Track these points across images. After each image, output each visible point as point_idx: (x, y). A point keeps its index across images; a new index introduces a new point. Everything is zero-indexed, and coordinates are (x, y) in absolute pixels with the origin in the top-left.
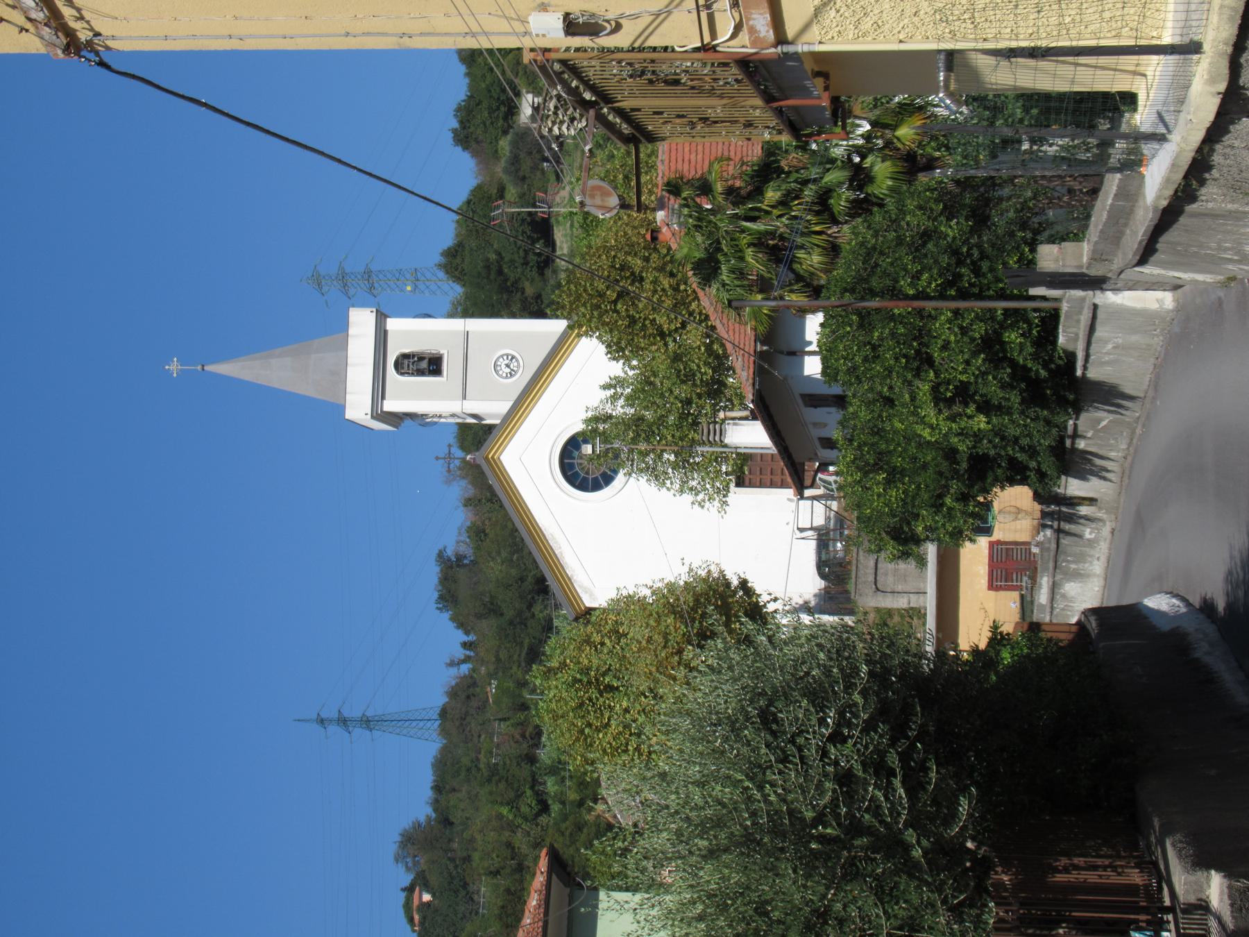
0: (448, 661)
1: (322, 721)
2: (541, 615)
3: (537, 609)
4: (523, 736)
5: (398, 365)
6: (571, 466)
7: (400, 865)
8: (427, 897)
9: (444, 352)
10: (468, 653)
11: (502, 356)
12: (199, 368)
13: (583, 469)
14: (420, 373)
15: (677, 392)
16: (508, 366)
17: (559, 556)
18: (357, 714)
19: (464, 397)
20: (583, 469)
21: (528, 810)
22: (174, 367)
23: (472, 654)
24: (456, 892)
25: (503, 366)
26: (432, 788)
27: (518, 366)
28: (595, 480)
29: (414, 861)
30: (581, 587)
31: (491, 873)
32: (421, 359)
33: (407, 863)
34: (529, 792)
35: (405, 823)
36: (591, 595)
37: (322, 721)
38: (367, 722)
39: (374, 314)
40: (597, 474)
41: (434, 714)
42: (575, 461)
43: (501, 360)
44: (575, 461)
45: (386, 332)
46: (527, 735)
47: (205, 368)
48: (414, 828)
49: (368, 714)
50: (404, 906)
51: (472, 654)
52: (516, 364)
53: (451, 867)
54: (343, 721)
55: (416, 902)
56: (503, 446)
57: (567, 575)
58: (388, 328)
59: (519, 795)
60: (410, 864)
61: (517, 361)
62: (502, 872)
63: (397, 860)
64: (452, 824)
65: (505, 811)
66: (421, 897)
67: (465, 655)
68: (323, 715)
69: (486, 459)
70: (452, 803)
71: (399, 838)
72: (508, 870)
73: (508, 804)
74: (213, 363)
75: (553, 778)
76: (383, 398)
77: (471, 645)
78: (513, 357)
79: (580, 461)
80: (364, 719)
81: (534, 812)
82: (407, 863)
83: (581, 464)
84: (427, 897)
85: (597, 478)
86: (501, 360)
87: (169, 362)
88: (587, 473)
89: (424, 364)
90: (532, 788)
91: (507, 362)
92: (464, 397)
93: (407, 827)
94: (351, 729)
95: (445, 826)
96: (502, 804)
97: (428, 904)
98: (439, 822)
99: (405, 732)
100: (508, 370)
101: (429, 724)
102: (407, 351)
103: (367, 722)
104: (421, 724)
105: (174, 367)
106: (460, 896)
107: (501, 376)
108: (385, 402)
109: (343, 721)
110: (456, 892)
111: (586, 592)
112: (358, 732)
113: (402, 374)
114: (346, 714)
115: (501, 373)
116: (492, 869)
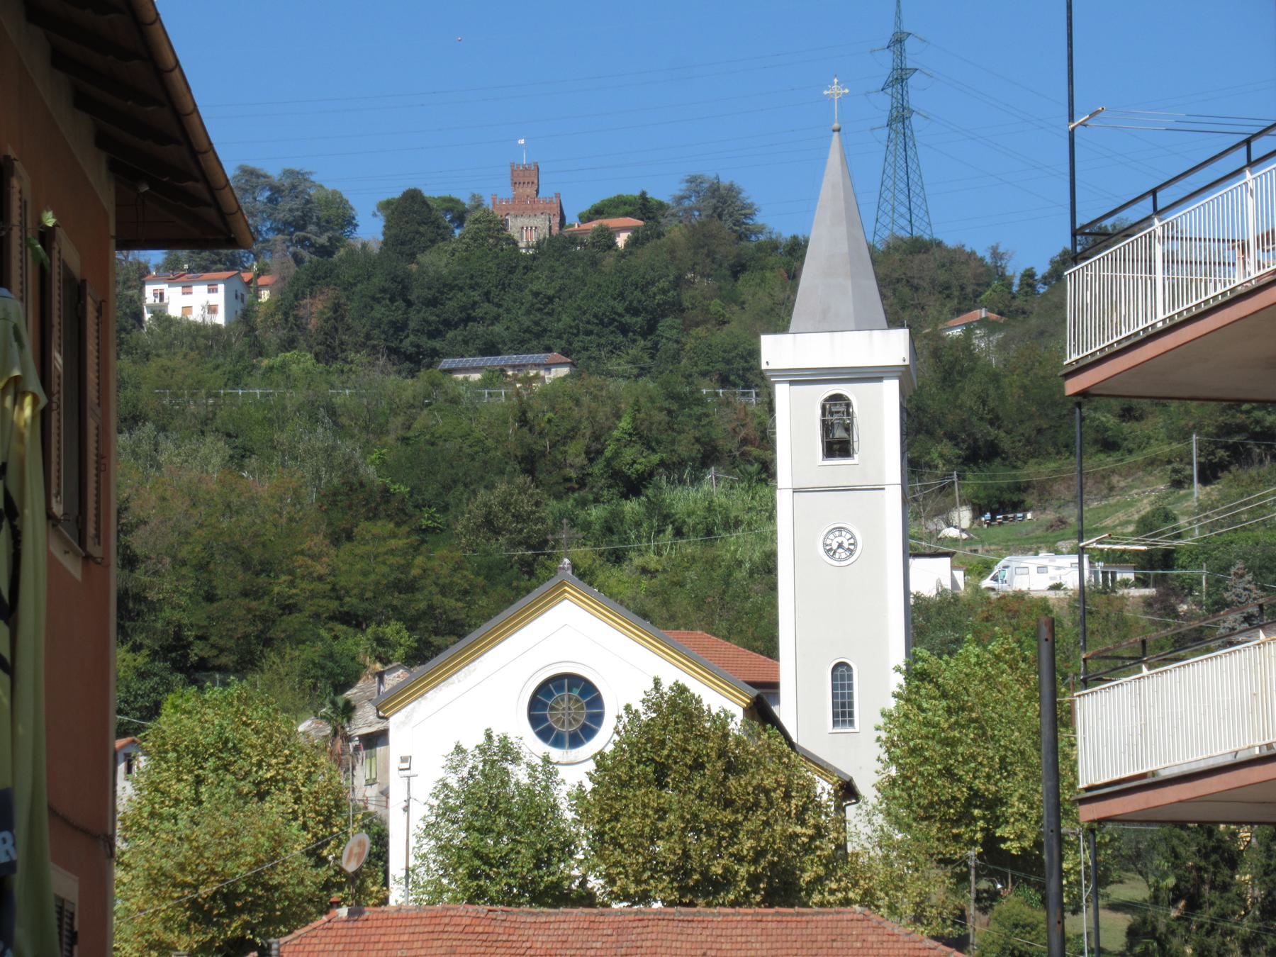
0: (1001, 250)
1: (898, 41)
2: (935, 455)
3: (947, 448)
4: (745, 441)
5: (837, 398)
6: (560, 688)
7: (684, 186)
8: (621, 240)
10: (1016, 281)
12: (836, 125)
14: (827, 428)
15: (626, 819)
16: (840, 546)
17: (450, 680)
21: (629, 459)
22: (836, 90)
23: (1015, 289)
24: (621, 297)
25: (840, 539)
27: (840, 560)
28: (544, 719)
29: (691, 209)
31: (524, 413)
32: (848, 429)
33: (689, 197)
34: (655, 458)
35: (752, 192)
36: (404, 723)
37: (898, 41)
38: (900, 117)
39: (901, 363)
40: (551, 721)
42: (566, 692)
44: (566, 692)
46: (748, 448)
48: (743, 208)
49: (915, 120)
51: (1015, 289)
52: (843, 556)
53: (663, 284)
54: (900, 78)
55: (612, 223)
56: (579, 603)
57: (427, 692)
58: (885, 382)
60: (686, 203)
61: (847, 558)
62: (525, 429)
63: (692, 180)
64: (735, 275)
65: (625, 424)
66: (624, 229)
67: (1013, 277)
68: (908, 43)
69: (562, 584)
71: (725, 181)
72: (529, 439)
73: (635, 429)
74: (841, 142)
75: (643, 510)
76: (792, 383)
77: (1030, 285)
79: (566, 699)
80: (906, 113)
81: (625, 469)
82: (689, 197)
83: (563, 700)
85: (547, 720)
88: (552, 708)
89: (839, 434)
90: (662, 463)
91: (846, 545)
94: (889, 90)
96: (634, 419)
97: (612, 245)
98: (738, 255)
99: (889, 183)
100: (835, 546)
101: (904, 223)
103: (900, 117)
105: (836, 90)
107: (826, 537)
109: (900, 78)
110: (621, 297)
111: (407, 717)
112: (885, 102)
113: (824, 408)
114: (913, 81)
115: (831, 536)
116: (530, 415)
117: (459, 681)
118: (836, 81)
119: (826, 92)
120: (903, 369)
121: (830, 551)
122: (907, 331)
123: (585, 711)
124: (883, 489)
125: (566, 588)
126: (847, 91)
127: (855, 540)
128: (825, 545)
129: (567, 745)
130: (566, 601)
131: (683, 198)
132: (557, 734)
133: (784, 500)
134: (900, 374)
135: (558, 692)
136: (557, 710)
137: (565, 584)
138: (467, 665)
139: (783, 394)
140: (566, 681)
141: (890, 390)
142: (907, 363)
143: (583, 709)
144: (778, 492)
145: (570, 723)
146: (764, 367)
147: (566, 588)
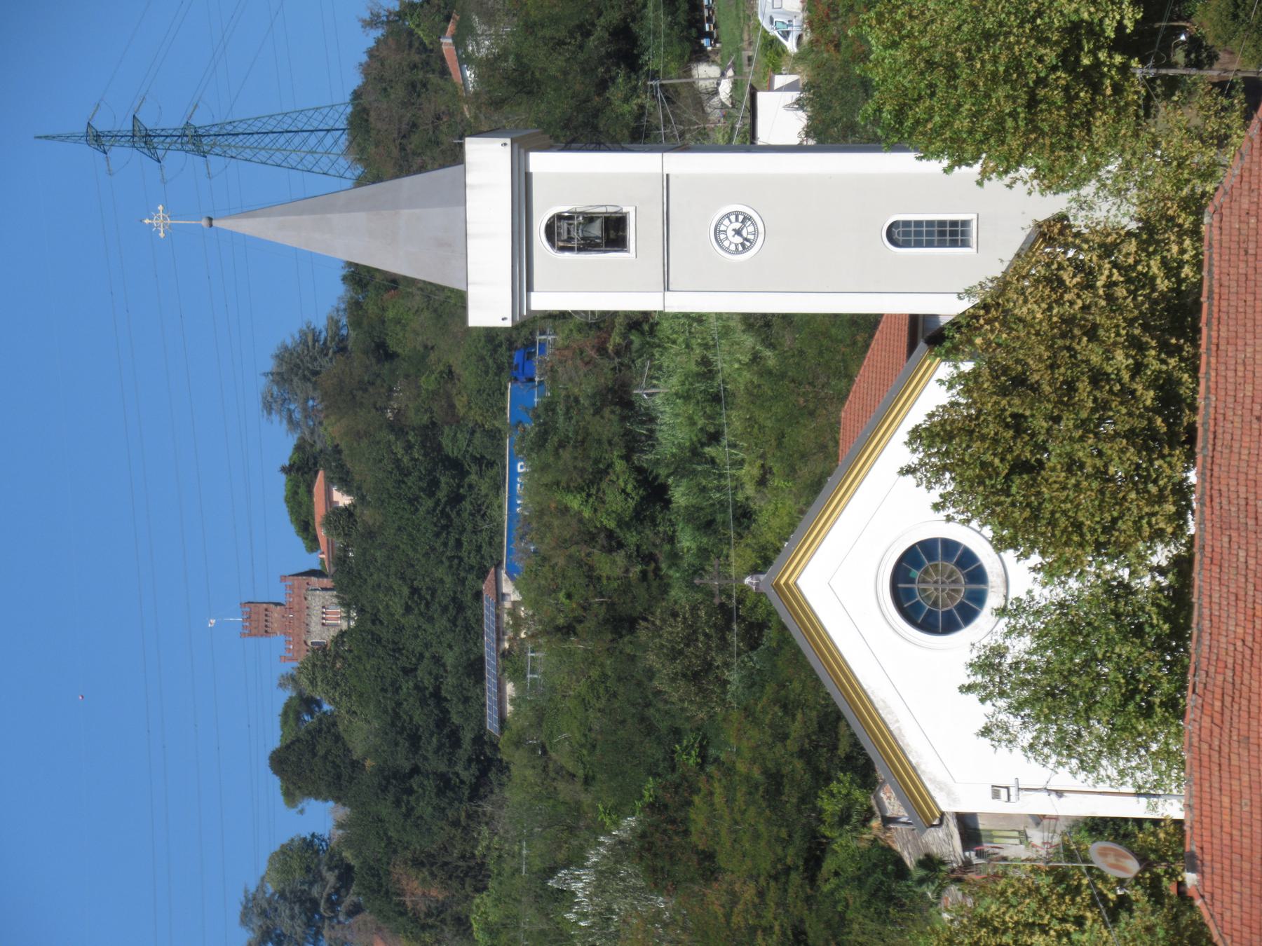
1: (97, 139)
2: (626, 108)
3: (616, 93)
4: (602, 350)
6: (910, 593)
7: (275, 417)
8: (342, 499)
9: (628, 209)
11: (727, 216)
13: (928, 597)
14: (588, 245)
16: (738, 232)
17: (896, 733)
18: (172, 121)
19: (667, 288)
20: (928, 597)
25: (730, 233)
26: (345, 279)
27: (756, 233)
28: (948, 615)
29: (305, 409)
30: (933, 781)
31: (558, 629)
32: (590, 218)
33: (290, 412)
34: (620, 465)
35: (287, 333)
36: (949, 794)
37: (97, 139)
39: (508, 148)
40: (951, 606)
41: (341, 115)
42: (915, 586)
43: (726, 222)
44: (915, 586)
45: (528, 176)
46: (610, 348)
47: (214, 223)
48: (305, 343)
49: (196, 122)
50: (287, 501)
52: (751, 229)
54: (144, 139)
55: (320, 510)
56: (801, 566)
57: (910, 762)
59: (602, 472)
60: (298, 416)
61: (754, 224)
62: (579, 628)
63: (268, 407)
64: (390, 356)
69: (777, 587)
70: (390, 314)
71: (270, 365)
72: (591, 623)
73: (580, 489)
74: (229, 216)
76: (530, 288)
78: (747, 218)
82: (290, 412)
83: (925, 590)
84: (342, 499)
85: (950, 612)
86: (726, 222)
87: (150, 212)
88: (935, 604)
89: (596, 230)
90: (627, 458)
91: (737, 225)
92: (667, 288)
93: (289, 343)
94: (160, 153)
95: (379, 361)
96: (568, 489)
99: (278, 157)
100: (738, 240)
101: (329, 139)
102: (563, 209)
104: (313, 140)
105: (159, 221)
106: (422, 510)
107: (727, 250)
108: (532, 294)
109: (144, 139)
110: (414, 501)
111: (941, 789)
112: (175, 159)
113: (562, 249)
114: (149, 122)
115: (726, 244)
116: (561, 621)
117: (897, 721)
118: (147, 221)
119: (162, 235)
120: (516, 146)
121: (745, 246)
122: (468, 140)
123: (940, 562)
124: (668, 175)
125: (782, 582)
126: (160, 208)
127: (742, 213)
128: (737, 252)
129: (982, 586)
130: (799, 582)
131: (290, 420)
132: (968, 599)
133: (678, 303)
134: (522, 151)
135: (915, 597)
136: (937, 598)
137: (777, 584)
138: (876, 710)
139: (542, 301)
140: (901, 585)
141: (542, 163)
142: (508, 141)
143: (936, 566)
144: (667, 310)
145: (954, 582)
146: (508, 324)
147: (782, 582)
